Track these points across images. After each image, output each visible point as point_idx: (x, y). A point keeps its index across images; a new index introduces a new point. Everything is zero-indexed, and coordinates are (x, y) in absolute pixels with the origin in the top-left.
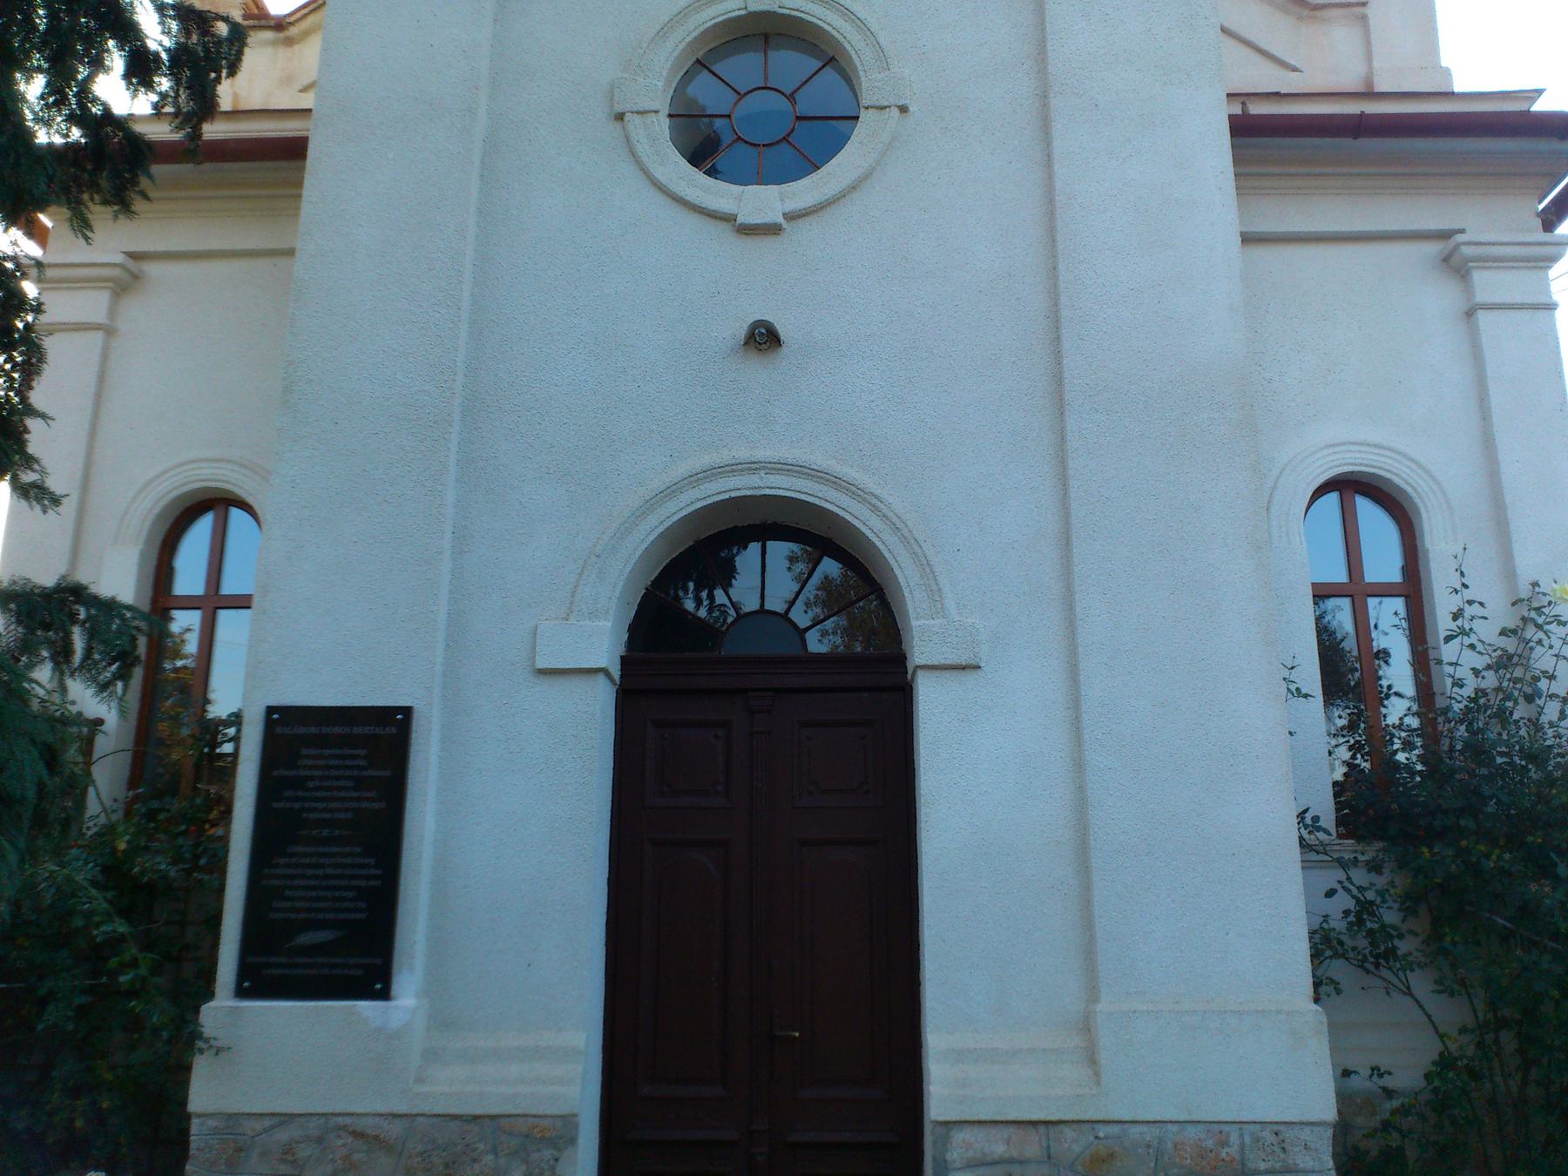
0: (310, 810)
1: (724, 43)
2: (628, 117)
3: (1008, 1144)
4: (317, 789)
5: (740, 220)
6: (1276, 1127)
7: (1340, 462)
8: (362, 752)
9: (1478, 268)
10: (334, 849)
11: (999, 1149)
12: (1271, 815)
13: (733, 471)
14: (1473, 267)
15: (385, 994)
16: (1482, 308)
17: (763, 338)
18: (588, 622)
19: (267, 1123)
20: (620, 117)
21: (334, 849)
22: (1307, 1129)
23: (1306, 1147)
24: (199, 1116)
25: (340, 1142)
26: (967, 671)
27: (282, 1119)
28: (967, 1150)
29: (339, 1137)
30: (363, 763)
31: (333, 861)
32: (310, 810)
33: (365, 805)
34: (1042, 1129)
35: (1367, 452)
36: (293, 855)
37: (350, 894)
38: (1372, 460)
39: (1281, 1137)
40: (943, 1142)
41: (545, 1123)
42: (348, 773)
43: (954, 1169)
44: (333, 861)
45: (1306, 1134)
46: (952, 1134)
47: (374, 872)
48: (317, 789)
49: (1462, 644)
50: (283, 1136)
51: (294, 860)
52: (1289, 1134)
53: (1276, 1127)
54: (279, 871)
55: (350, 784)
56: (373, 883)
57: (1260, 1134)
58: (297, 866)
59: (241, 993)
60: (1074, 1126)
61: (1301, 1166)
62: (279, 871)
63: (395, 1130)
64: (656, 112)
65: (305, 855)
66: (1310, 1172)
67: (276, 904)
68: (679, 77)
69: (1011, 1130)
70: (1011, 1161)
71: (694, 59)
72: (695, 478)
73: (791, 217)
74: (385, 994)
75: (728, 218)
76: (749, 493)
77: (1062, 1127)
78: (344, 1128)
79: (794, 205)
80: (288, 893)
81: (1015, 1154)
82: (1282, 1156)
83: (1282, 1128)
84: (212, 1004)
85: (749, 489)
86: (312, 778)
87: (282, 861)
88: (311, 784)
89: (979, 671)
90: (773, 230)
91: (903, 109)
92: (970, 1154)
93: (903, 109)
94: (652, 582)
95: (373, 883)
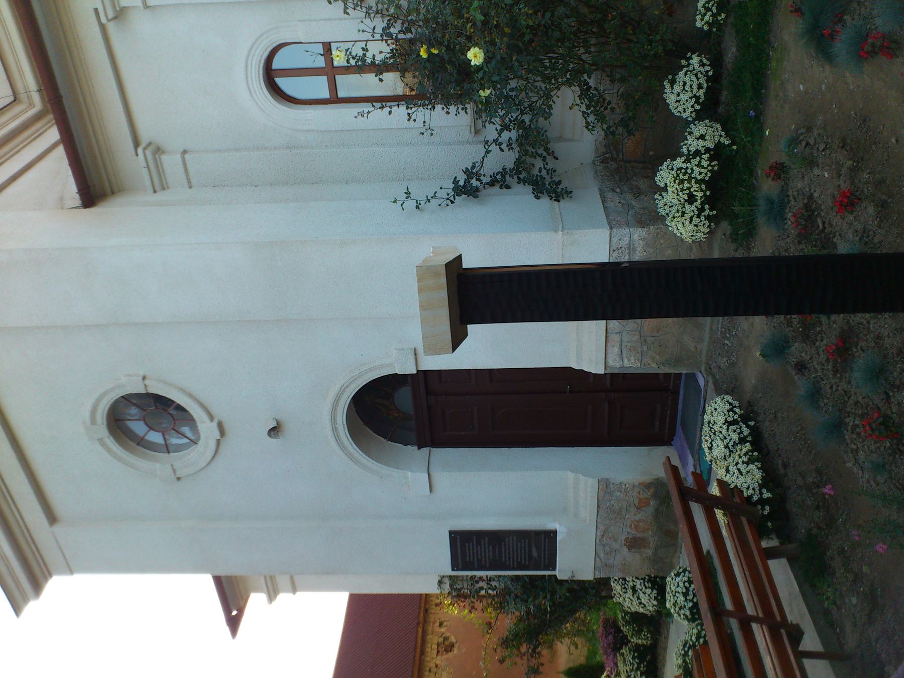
0: (489, 557)
1: (123, 432)
2: (178, 476)
3: (614, 346)
4: (481, 555)
5: (218, 437)
6: (611, 252)
7: (260, 90)
8: (467, 544)
9: (118, 3)
10: (503, 550)
11: (616, 350)
12: (474, 245)
13: (338, 436)
14: (119, 7)
15: (555, 533)
16: (146, 3)
17: (275, 431)
18: (409, 479)
19: (597, 559)
20: (179, 479)
21: (503, 550)
22: (613, 239)
23: (620, 240)
24: (594, 576)
25: (605, 540)
26: (417, 353)
27: (596, 556)
28: (616, 360)
29: (603, 541)
30: (471, 544)
31: (507, 550)
32: (489, 557)
33: (487, 542)
34: (608, 335)
35: (252, 78)
36: (505, 560)
37: (519, 544)
38: (260, 94)
39: (616, 249)
40: (611, 367)
41: (600, 487)
42: (475, 547)
43: (623, 364)
44: (507, 550)
45: (615, 240)
46: (609, 365)
47: (511, 539)
48: (481, 555)
49: (367, 41)
50: (602, 555)
51: (508, 560)
52: (614, 246)
53: (611, 252)
54: (512, 564)
55: (479, 547)
56: (515, 538)
57: (614, 258)
58: (509, 559)
59: (554, 569)
60: (608, 324)
61: (628, 242)
62: (512, 564)
63: (601, 527)
64: (172, 465)
65: (505, 557)
66: (630, 239)
67: (523, 563)
68: (149, 452)
69: (609, 344)
70: (621, 345)
71: (137, 446)
72: (343, 449)
73: (211, 418)
74: (555, 533)
75: (218, 442)
76: (346, 430)
77: (608, 328)
78: (600, 540)
79: (205, 417)
80: (519, 560)
81: (618, 344)
82: (623, 249)
83: (611, 249)
84: (558, 576)
85: (345, 430)
86: (477, 558)
87: (508, 563)
88: (480, 557)
89: (416, 348)
90: (220, 426)
91: (144, 378)
92: (618, 359)
93: (144, 378)
94: (385, 438)
95: (515, 538)
